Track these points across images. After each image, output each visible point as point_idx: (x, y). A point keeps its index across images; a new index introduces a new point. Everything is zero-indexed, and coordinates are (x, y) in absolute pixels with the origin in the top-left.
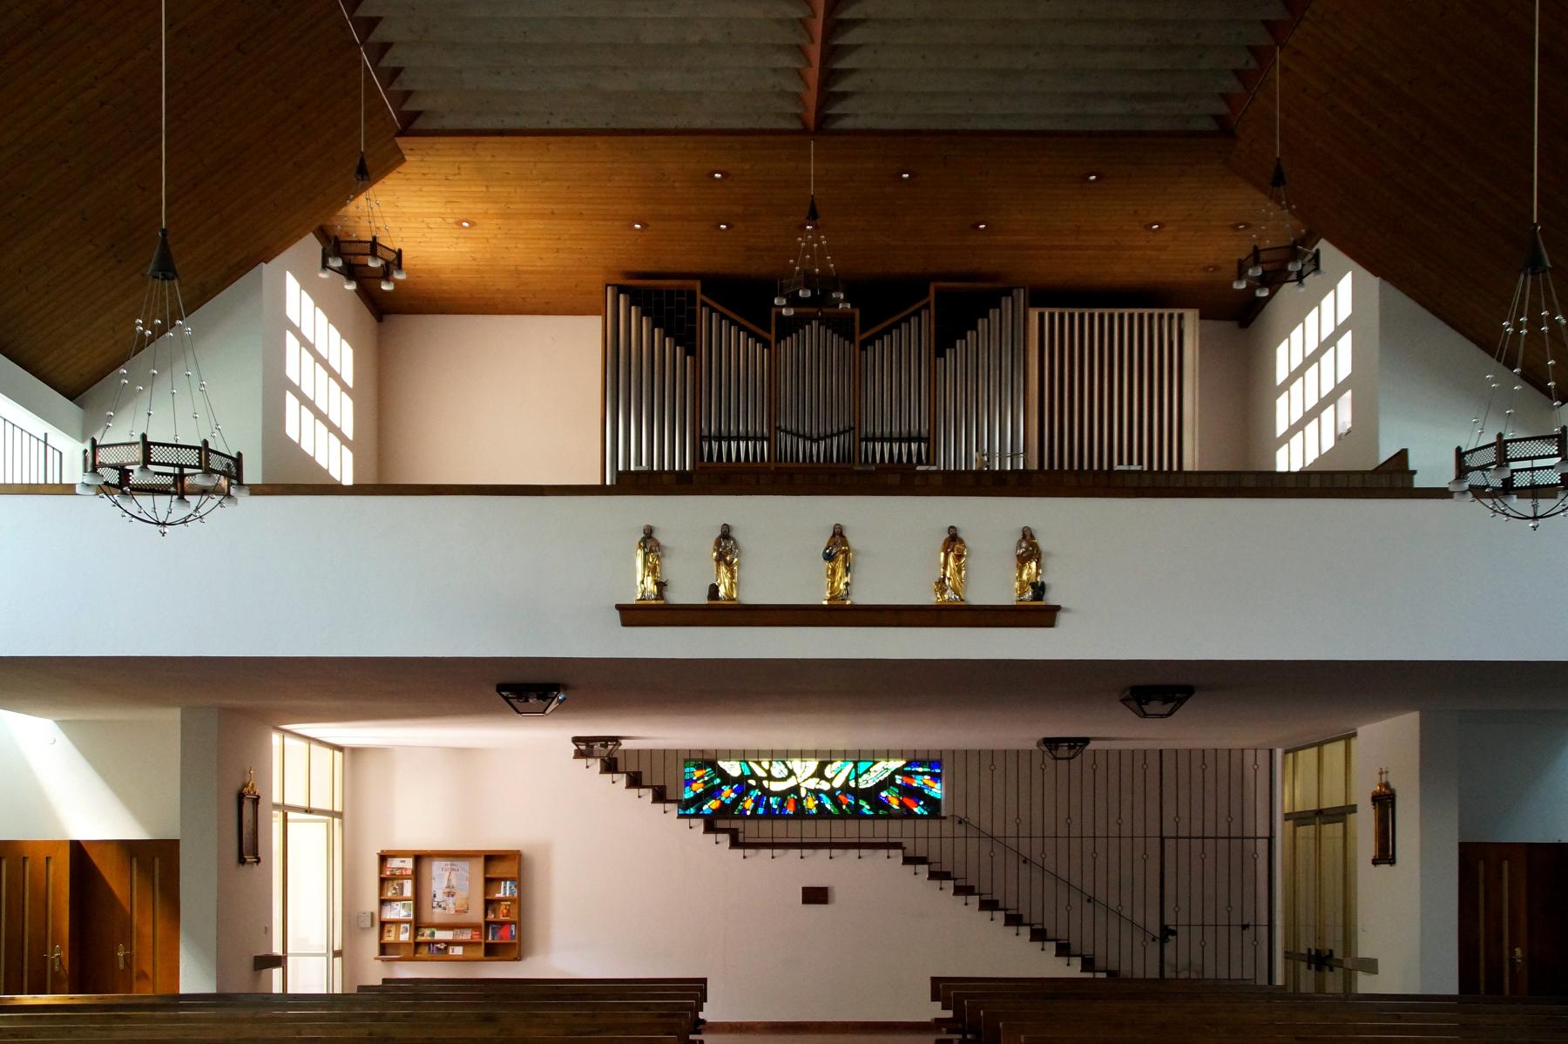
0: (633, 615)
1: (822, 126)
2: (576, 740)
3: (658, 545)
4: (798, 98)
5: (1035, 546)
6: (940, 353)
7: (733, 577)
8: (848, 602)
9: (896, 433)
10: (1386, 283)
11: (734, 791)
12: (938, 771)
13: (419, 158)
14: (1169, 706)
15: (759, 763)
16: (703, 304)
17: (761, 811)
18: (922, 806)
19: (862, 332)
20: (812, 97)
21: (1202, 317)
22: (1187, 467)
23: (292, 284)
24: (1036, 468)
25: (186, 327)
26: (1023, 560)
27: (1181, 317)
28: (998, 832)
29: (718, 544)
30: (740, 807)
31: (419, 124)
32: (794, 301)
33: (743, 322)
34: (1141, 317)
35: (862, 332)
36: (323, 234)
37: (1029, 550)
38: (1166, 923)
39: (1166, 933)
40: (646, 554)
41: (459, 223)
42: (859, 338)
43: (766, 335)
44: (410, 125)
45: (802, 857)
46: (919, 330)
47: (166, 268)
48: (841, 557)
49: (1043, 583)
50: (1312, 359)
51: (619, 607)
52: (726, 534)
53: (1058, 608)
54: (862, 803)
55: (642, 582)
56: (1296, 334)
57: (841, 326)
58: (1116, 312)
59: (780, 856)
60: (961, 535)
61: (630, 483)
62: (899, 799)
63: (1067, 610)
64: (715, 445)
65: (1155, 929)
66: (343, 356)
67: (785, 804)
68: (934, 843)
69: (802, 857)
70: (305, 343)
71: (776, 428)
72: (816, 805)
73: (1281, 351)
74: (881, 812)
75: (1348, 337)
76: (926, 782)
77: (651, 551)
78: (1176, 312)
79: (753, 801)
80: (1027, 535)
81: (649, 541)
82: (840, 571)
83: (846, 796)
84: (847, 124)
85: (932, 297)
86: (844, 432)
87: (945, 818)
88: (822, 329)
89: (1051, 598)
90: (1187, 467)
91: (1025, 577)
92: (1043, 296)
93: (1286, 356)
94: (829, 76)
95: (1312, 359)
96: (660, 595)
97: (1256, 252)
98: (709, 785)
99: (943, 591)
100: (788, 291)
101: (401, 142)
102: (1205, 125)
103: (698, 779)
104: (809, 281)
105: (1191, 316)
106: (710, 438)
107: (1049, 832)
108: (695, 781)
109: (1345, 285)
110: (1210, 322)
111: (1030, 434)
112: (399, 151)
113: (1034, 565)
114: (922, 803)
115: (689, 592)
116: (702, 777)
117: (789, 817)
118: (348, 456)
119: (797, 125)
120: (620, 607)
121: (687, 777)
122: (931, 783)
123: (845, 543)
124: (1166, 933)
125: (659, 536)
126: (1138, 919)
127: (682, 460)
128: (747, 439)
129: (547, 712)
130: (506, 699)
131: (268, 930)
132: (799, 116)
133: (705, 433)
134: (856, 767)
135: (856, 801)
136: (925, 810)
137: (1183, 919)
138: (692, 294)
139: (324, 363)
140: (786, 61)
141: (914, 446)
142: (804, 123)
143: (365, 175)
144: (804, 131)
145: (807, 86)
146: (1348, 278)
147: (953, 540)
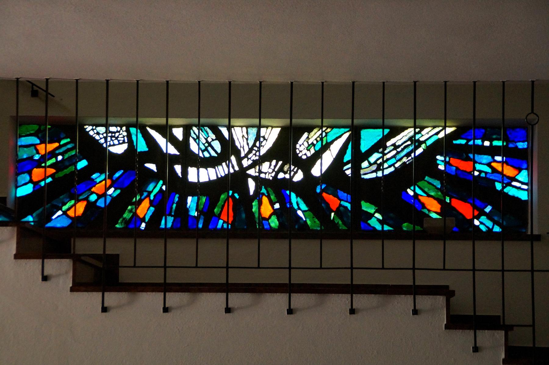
11: (115, 184)
12: (522, 145)
15: (165, 131)
17: (168, 222)
18: (489, 216)
30: (127, 215)
45: (228, 310)
54: (367, 207)
59: (119, 307)
62: (441, 201)
67: (216, 210)
69: (290, 311)
72: (275, 212)
74: (405, 226)
76: (499, 167)
79: (152, 203)
83: (336, 196)
87: (538, 238)
98: (67, 171)
103: (44, 159)
108: (38, 164)
114: (488, 209)
116: (53, 154)
117: (167, 234)
121: (24, 154)
122: (509, 171)
134: (355, 139)
135: (356, 206)
136: (495, 223)
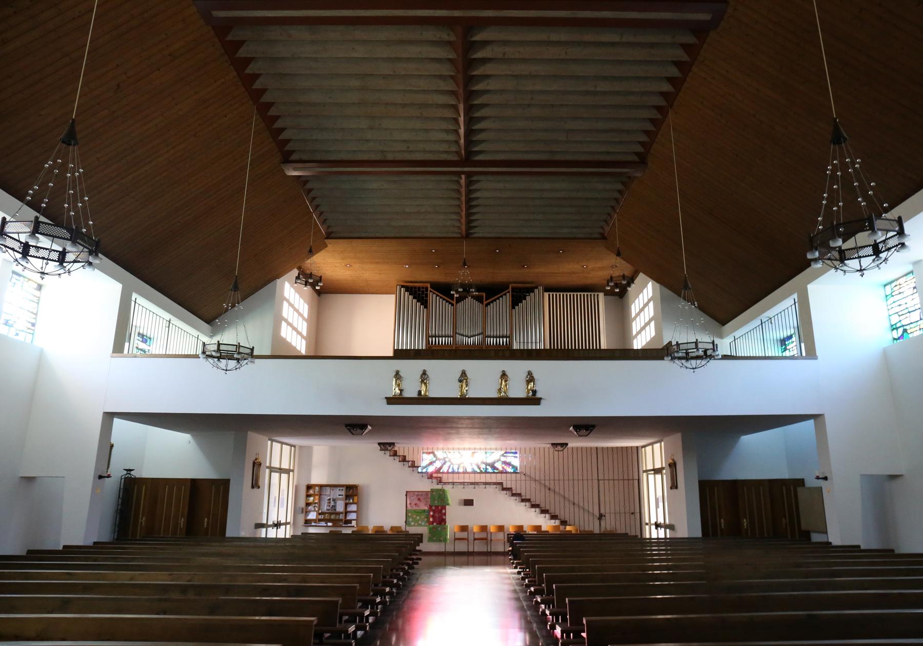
0: (391, 401)
1: (468, 236)
2: (379, 444)
3: (401, 377)
4: (459, 227)
5: (533, 377)
6: (513, 307)
7: (426, 388)
8: (467, 397)
9: (495, 335)
10: (662, 286)
13: (332, 245)
14: (588, 432)
16: (431, 291)
19: (486, 300)
20: (464, 228)
21: (605, 295)
22: (602, 347)
23: (287, 286)
24: (549, 348)
25: (240, 307)
26: (528, 382)
27: (598, 295)
28: (537, 478)
29: (422, 376)
31: (332, 235)
32: (457, 292)
33: (444, 297)
34: (584, 295)
35: (486, 300)
36: (299, 268)
37: (530, 378)
38: (601, 512)
39: (601, 516)
40: (396, 380)
41: (346, 265)
42: (485, 303)
43: (451, 301)
44: (329, 236)
46: (506, 300)
47: (236, 288)
48: (465, 381)
49: (536, 390)
50: (642, 310)
51: (386, 398)
52: (424, 373)
53: (541, 398)
55: (395, 389)
56: (637, 301)
57: (479, 299)
58: (575, 294)
60: (507, 373)
61: (399, 354)
63: (544, 399)
64: (434, 339)
65: (598, 515)
66: (304, 308)
68: (514, 483)
70: (291, 305)
71: (456, 333)
73: (633, 306)
75: (652, 303)
77: (398, 379)
78: (596, 294)
80: (530, 373)
81: (397, 375)
82: (464, 386)
84: (476, 235)
85: (510, 289)
86: (479, 334)
88: (474, 301)
89: (538, 395)
90: (602, 347)
91: (529, 388)
92: (547, 289)
93: (634, 308)
94: (469, 222)
95: (642, 310)
96: (401, 394)
97: (611, 277)
99: (500, 393)
100: (455, 289)
101: (327, 241)
102: (597, 236)
104: (462, 285)
105: (601, 295)
106: (432, 337)
107: (557, 478)
109: (650, 285)
110: (607, 297)
111: (546, 337)
112: (326, 243)
113: (532, 383)
115: (411, 393)
118: (304, 342)
119: (460, 236)
120: (386, 398)
123: (466, 376)
124: (601, 516)
125: (401, 374)
126: (591, 510)
127: (421, 345)
128: (445, 337)
129: (363, 434)
130: (348, 429)
131: (261, 513)
132: (460, 233)
133: (430, 335)
137: (608, 511)
138: (427, 288)
139: (297, 311)
140: (454, 217)
141: (505, 340)
142: (462, 235)
143: (311, 252)
144: (462, 237)
145: (462, 224)
146: (650, 283)
147: (504, 375)
